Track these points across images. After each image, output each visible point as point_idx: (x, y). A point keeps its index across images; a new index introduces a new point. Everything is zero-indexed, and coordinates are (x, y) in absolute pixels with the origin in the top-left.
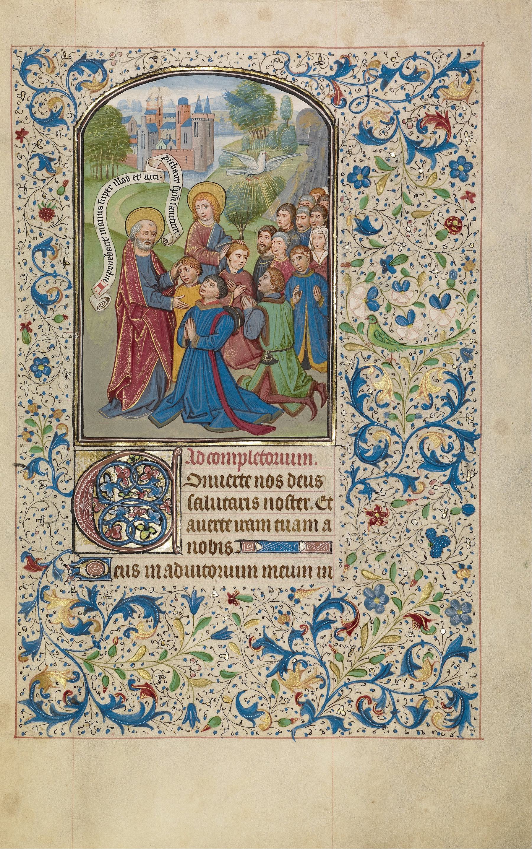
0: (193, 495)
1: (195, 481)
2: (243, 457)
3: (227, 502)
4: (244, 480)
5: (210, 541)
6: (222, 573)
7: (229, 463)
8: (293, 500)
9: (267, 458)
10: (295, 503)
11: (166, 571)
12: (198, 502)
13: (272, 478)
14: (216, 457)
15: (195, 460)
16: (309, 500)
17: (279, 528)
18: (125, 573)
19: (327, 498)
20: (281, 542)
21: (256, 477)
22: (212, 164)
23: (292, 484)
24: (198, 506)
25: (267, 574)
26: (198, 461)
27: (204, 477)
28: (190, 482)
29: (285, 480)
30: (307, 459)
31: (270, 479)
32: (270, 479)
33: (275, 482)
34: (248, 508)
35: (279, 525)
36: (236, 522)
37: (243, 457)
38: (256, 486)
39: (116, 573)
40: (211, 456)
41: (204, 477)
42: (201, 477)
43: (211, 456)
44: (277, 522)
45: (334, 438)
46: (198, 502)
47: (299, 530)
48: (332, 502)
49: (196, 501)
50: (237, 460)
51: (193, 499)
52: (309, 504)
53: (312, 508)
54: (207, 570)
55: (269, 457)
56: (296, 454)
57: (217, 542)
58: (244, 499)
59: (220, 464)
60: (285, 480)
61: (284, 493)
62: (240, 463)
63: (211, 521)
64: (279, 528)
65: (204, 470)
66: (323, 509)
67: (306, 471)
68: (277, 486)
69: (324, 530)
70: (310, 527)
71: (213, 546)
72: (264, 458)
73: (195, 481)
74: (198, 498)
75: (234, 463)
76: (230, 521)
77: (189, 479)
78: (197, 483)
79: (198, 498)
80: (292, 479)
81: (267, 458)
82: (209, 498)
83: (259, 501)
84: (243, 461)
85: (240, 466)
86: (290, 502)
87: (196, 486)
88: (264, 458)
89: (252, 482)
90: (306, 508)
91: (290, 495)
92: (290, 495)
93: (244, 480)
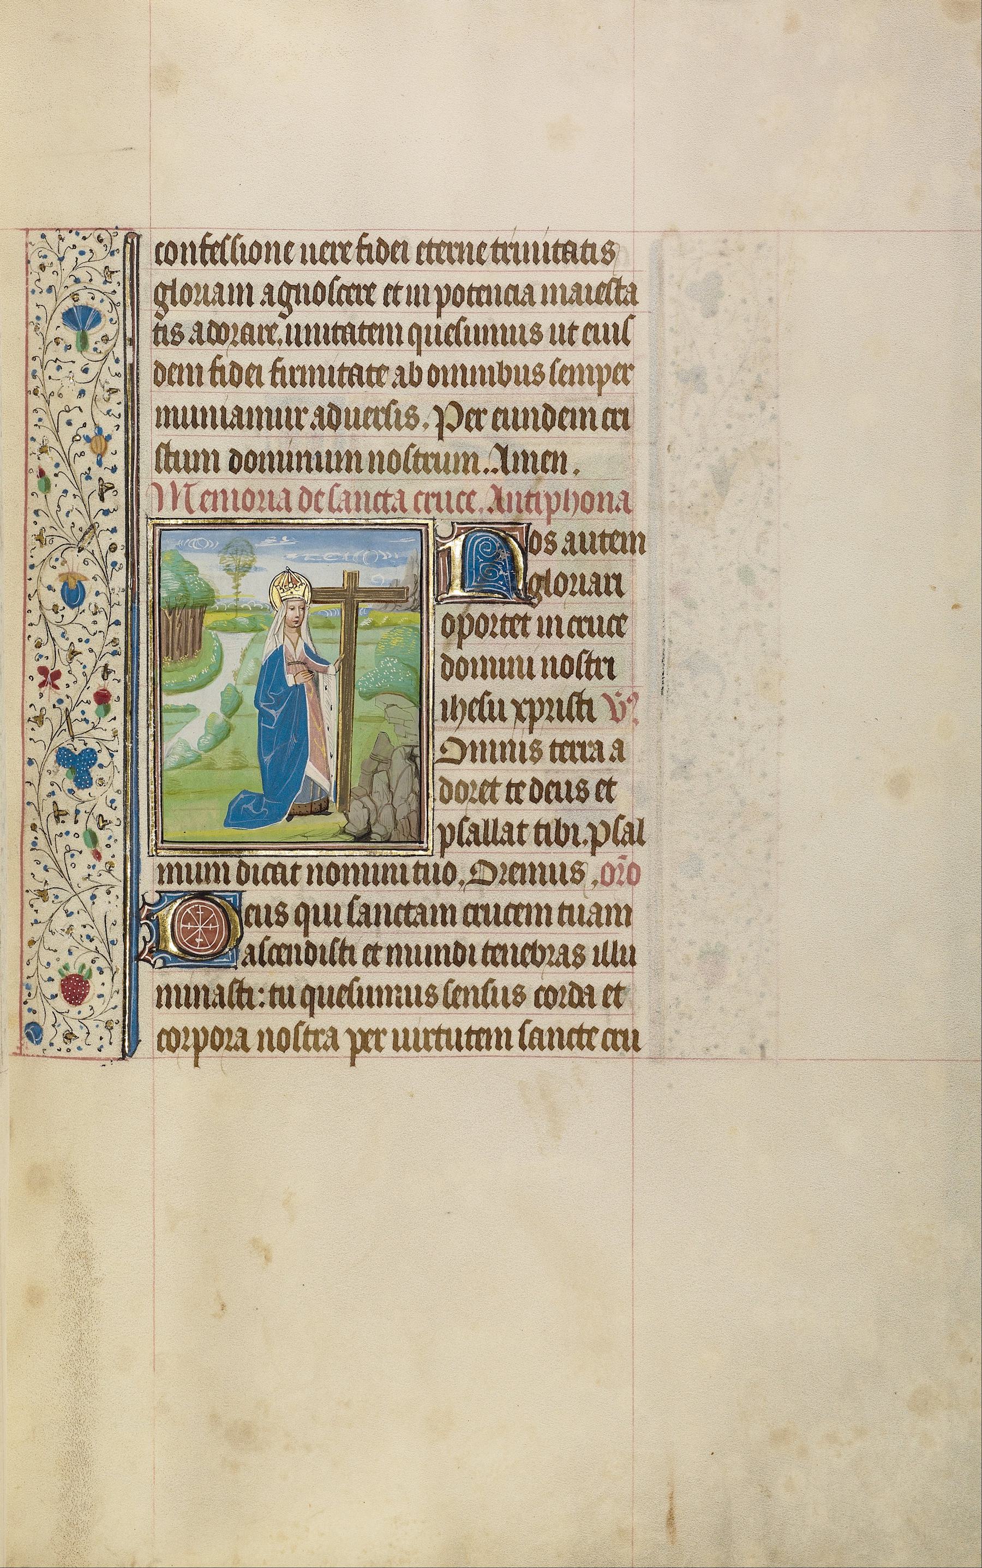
0: (337, 485)
1: (454, 751)
2: (554, 499)
4: (585, 1036)
5: (558, 822)
6: (554, 714)
9: (169, 1040)
11: (526, 294)
12: (536, 1035)
24: (536, 1042)
27: (473, 743)
33: (544, 545)
37: (554, 499)
41: (473, 743)
42: (467, 743)
46: (536, 1035)
48: (629, 372)
49: (532, 1034)
50: (595, 378)
51: (466, 825)
59: (256, 473)
63: (368, 410)
68: (547, 551)
73: (454, 751)
74: (536, 1029)
76: (595, 1030)
77: (443, 750)
78: (457, 756)
79: (536, 1029)
80: (305, 497)
81: (169, 1040)
86: (337, 952)
91: (585, 651)
92: (585, 651)
93: (585, 1036)
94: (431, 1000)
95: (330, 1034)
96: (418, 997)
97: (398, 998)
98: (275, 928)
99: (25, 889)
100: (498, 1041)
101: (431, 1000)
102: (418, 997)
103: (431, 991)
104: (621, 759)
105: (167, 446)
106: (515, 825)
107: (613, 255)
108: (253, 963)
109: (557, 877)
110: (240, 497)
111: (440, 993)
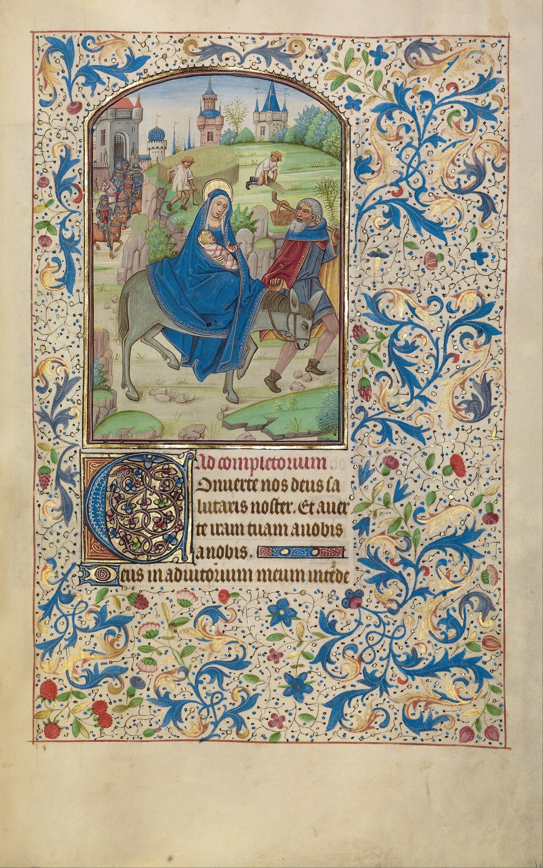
2: (255, 462)
3: (205, 574)
5: (227, 547)
7: (319, 468)
8: (277, 504)
10: (279, 507)
13: (278, 482)
14: (227, 462)
15: (206, 465)
16: (292, 503)
17: (252, 531)
18: (130, 577)
19: (309, 503)
20: (329, 547)
21: (263, 481)
22: (101, 199)
23: (295, 488)
25: (152, 578)
26: (209, 467)
28: (201, 487)
29: (289, 484)
30: (322, 464)
31: (276, 483)
32: (276, 483)
33: (281, 487)
34: (237, 511)
35: (252, 528)
36: (212, 526)
37: (255, 462)
38: (263, 490)
39: (122, 577)
40: (222, 462)
43: (222, 462)
44: (250, 526)
45: (345, 442)
47: (298, 535)
50: (249, 465)
51: (332, 481)
52: (291, 508)
53: (294, 512)
54: (205, 574)
55: (281, 462)
56: (310, 457)
57: (234, 547)
58: (233, 503)
60: (289, 484)
61: (268, 496)
62: (252, 468)
64: (252, 531)
65: (215, 474)
66: (304, 513)
67: (322, 475)
68: (283, 490)
69: (292, 534)
70: (235, 463)
71: (229, 551)
72: (276, 462)
73: (205, 485)
75: (246, 468)
76: (205, 525)
82: (202, 502)
83: (247, 504)
84: (255, 466)
85: (252, 472)
86: (274, 506)
87: (207, 491)
88: (276, 462)
89: (259, 486)
90: (289, 512)
91: (274, 499)
92: (274, 499)
93: (251, 484)
94: (320, 488)
95: (225, 526)
96: (313, 487)
97: (290, 463)
98: (137, 582)
99: (503, 421)
100: (235, 463)
101: (320, 488)
102: (313, 487)
103: (320, 483)
104: (338, 490)
105: (277, 500)
106: (199, 571)
107: (341, 530)
108: (324, 512)
109: (225, 578)
110: (183, 577)
111: (325, 485)
